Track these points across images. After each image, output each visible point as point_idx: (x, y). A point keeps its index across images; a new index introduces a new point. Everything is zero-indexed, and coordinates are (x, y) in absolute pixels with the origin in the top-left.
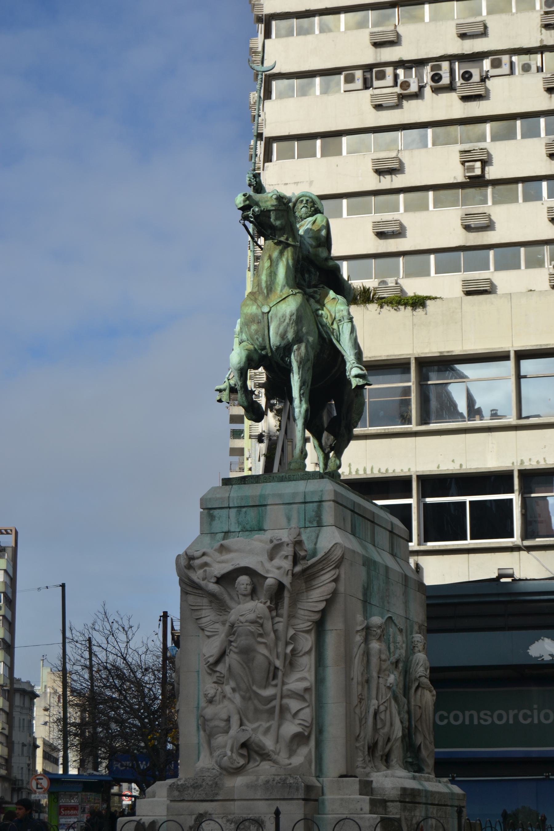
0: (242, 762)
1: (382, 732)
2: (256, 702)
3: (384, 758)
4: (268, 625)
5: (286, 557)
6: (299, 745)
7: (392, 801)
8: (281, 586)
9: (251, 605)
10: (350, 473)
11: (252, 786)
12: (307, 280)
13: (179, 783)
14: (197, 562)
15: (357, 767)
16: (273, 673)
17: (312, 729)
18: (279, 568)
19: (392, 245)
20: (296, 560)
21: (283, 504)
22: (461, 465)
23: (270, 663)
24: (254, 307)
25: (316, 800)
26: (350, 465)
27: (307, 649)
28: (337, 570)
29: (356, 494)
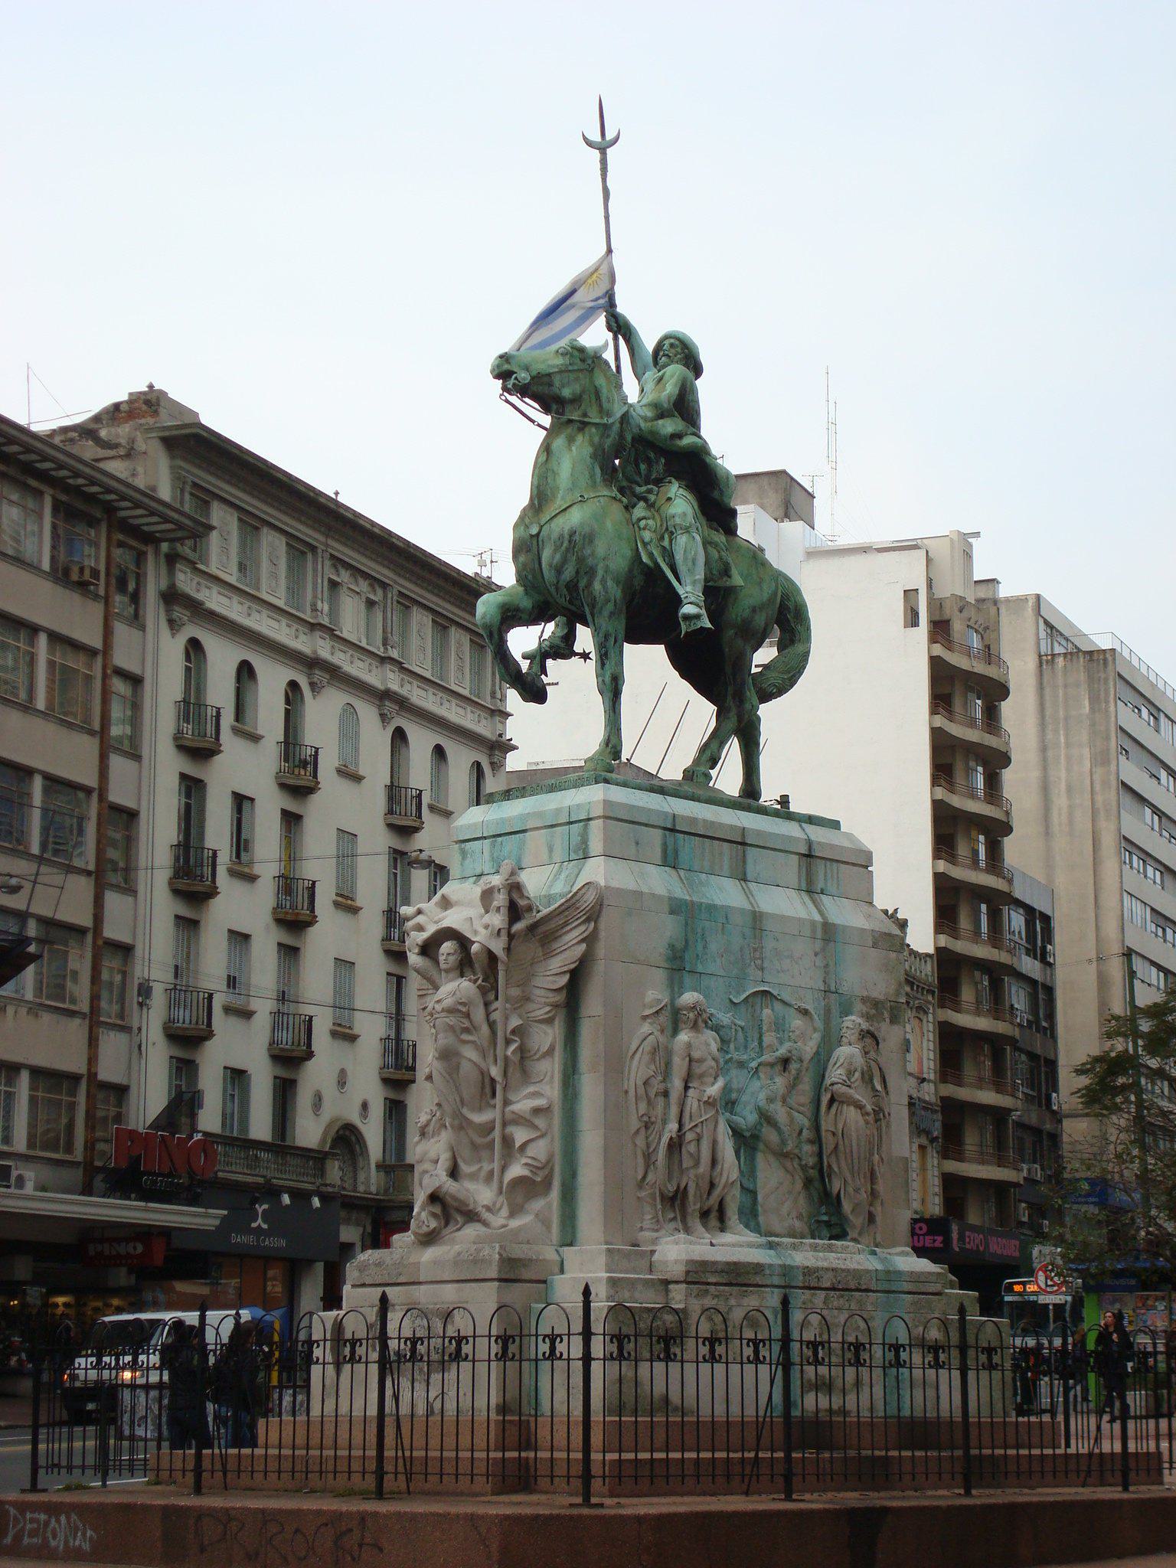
0: (433, 1224)
2: (470, 1132)
3: (714, 1215)
4: (479, 1015)
7: (677, 1282)
16: (488, 1088)
20: (515, 912)
21: (546, 827)
25: (545, 1282)
27: (545, 1048)
29: (253, 824)
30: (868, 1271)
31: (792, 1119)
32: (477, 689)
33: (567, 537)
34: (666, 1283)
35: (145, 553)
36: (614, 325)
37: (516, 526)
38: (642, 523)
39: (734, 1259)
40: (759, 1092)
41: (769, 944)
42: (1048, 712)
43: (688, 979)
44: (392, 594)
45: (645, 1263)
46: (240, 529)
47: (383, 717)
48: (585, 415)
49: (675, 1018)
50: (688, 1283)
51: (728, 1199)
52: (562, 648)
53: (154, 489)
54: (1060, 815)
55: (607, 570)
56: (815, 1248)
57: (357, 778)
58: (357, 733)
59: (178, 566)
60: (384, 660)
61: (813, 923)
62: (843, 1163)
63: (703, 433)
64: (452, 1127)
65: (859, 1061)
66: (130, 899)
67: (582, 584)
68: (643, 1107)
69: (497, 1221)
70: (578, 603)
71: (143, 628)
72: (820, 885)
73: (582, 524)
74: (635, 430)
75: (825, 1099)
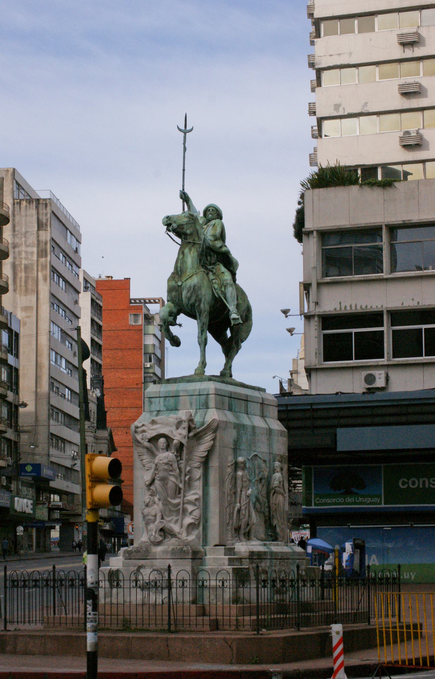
0: (161, 539)
1: (244, 520)
2: (170, 507)
3: (247, 534)
4: (175, 465)
5: (184, 428)
6: (192, 530)
8: (181, 445)
9: (166, 454)
10: (341, 309)
11: (164, 552)
12: (209, 260)
13: (129, 549)
14: (140, 430)
15: (228, 540)
16: (178, 491)
18: (180, 434)
19: (415, 103)
20: (190, 430)
22: (418, 303)
24: (174, 282)
25: (201, 559)
26: (340, 303)
27: (198, 477)
33: (192, 287)
34: (241, 559)
36: (184, 197)
37: (169, 280)
38: (214, 281)
48: (194, 240)
54: (21, 281)
63: (227, 243)
67: (197, 304)
70: (193, 311)
72: (265, 414)
73: (198, 283)
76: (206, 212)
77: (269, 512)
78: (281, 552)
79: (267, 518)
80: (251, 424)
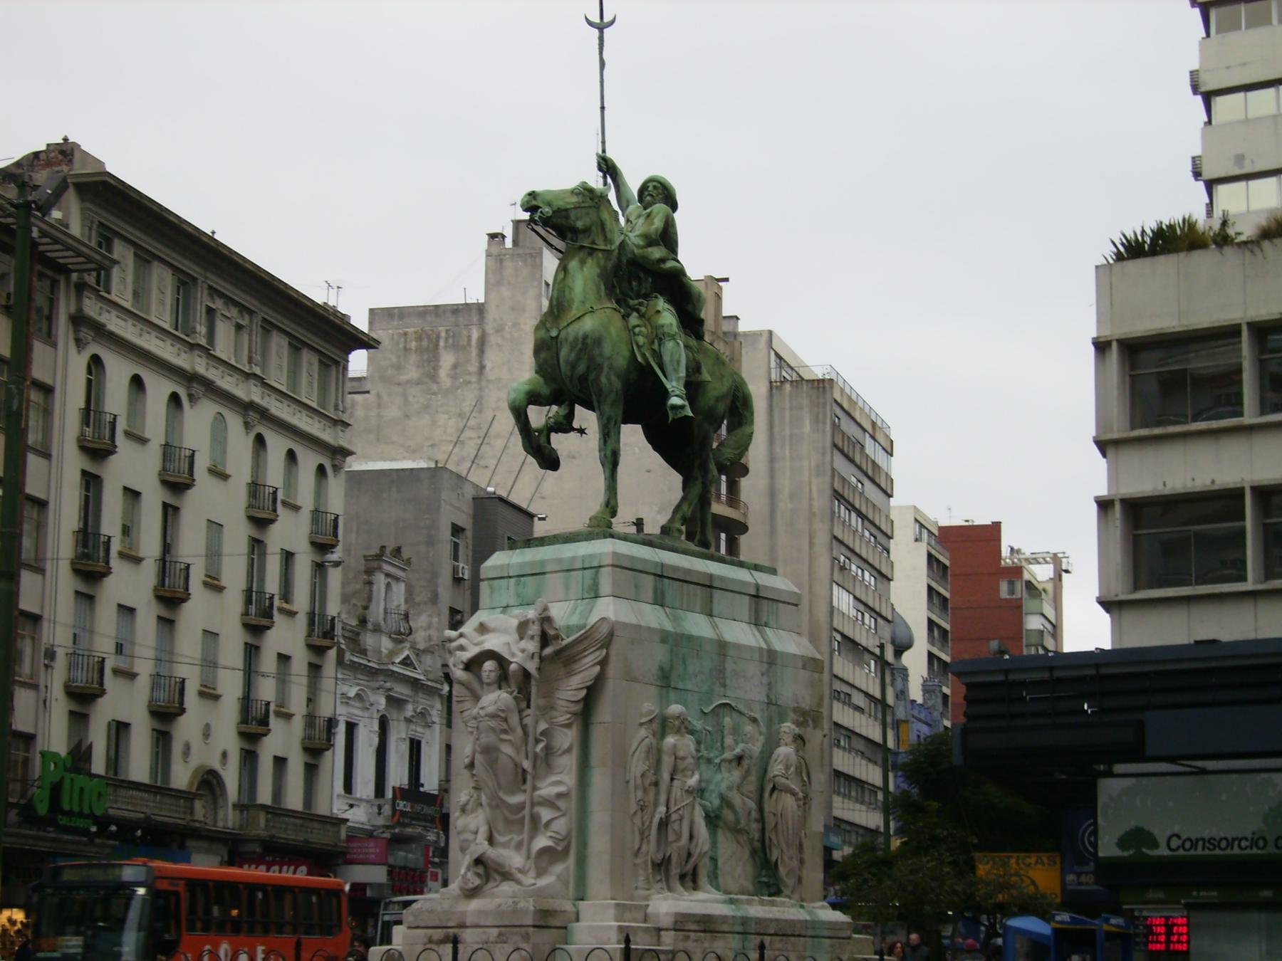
0: (477, 882)
2: (505, 811)
3: (689, 877)
4: (514, 719)
7: (667, 930)
17: (569, 842)
18: (523, 651)
20: (545, 640)
23: (516, 765)
27: (566, 746)
28: (604, 651)
30: (800, 921)
31: (744, 803)
32: (322, 402)
34: (660, 930)
35: (58, 282)
37: (537, 329)
38: (637, 330)
39: (707, 912)
40: (726, 779)
41: (729, 665)
42: (777, 430)
43: (672, 695)
44: (257, 319)
45: (640, 915)
46: (135, 262)
47: (247, 425)
48: (593, 243)
49: (663, 725)
50: (676, 930)
51: (701, 865)
52: (565, 425)
53: (67, 226)
55: (611, 367)
56: (762, 903)
57: (224, 477)
58: (225, 438)
59: (85, 293)
60: (249, 376)
61: (761, 649)
62: (781, 838)
63: (681, 256)
64: (490, 805)
65: (793, 758)
66: (40, 577)
67: (592, 377)
68: (640, 794)
69: (528, 880)
71: (54, 345)
72: (765, 619)
74: (630, 255)
75: (769, 787)
76: (643, 190)
77: (763, 830)
78: (777, 920)
79: (757, 845)
80: (715, 637)
